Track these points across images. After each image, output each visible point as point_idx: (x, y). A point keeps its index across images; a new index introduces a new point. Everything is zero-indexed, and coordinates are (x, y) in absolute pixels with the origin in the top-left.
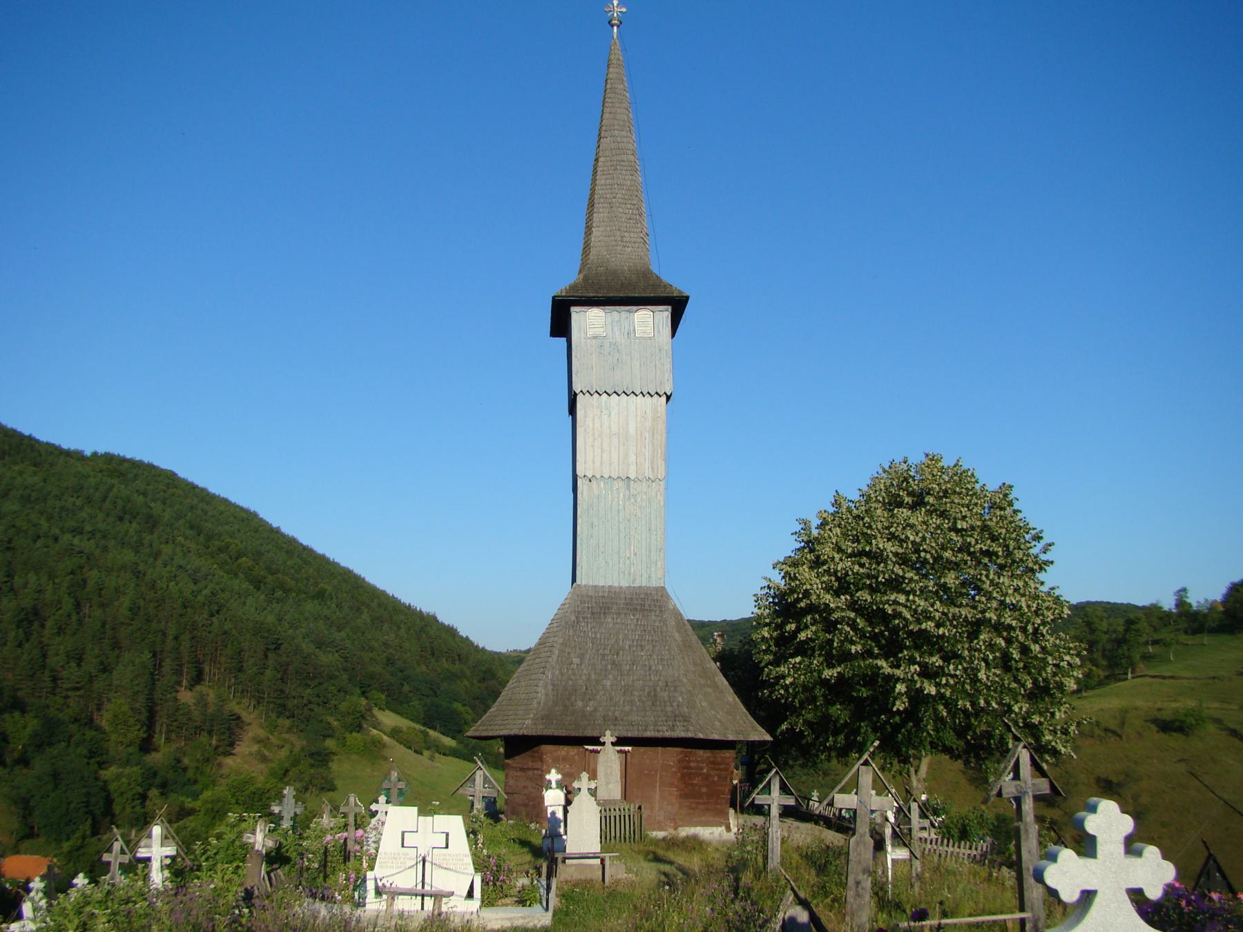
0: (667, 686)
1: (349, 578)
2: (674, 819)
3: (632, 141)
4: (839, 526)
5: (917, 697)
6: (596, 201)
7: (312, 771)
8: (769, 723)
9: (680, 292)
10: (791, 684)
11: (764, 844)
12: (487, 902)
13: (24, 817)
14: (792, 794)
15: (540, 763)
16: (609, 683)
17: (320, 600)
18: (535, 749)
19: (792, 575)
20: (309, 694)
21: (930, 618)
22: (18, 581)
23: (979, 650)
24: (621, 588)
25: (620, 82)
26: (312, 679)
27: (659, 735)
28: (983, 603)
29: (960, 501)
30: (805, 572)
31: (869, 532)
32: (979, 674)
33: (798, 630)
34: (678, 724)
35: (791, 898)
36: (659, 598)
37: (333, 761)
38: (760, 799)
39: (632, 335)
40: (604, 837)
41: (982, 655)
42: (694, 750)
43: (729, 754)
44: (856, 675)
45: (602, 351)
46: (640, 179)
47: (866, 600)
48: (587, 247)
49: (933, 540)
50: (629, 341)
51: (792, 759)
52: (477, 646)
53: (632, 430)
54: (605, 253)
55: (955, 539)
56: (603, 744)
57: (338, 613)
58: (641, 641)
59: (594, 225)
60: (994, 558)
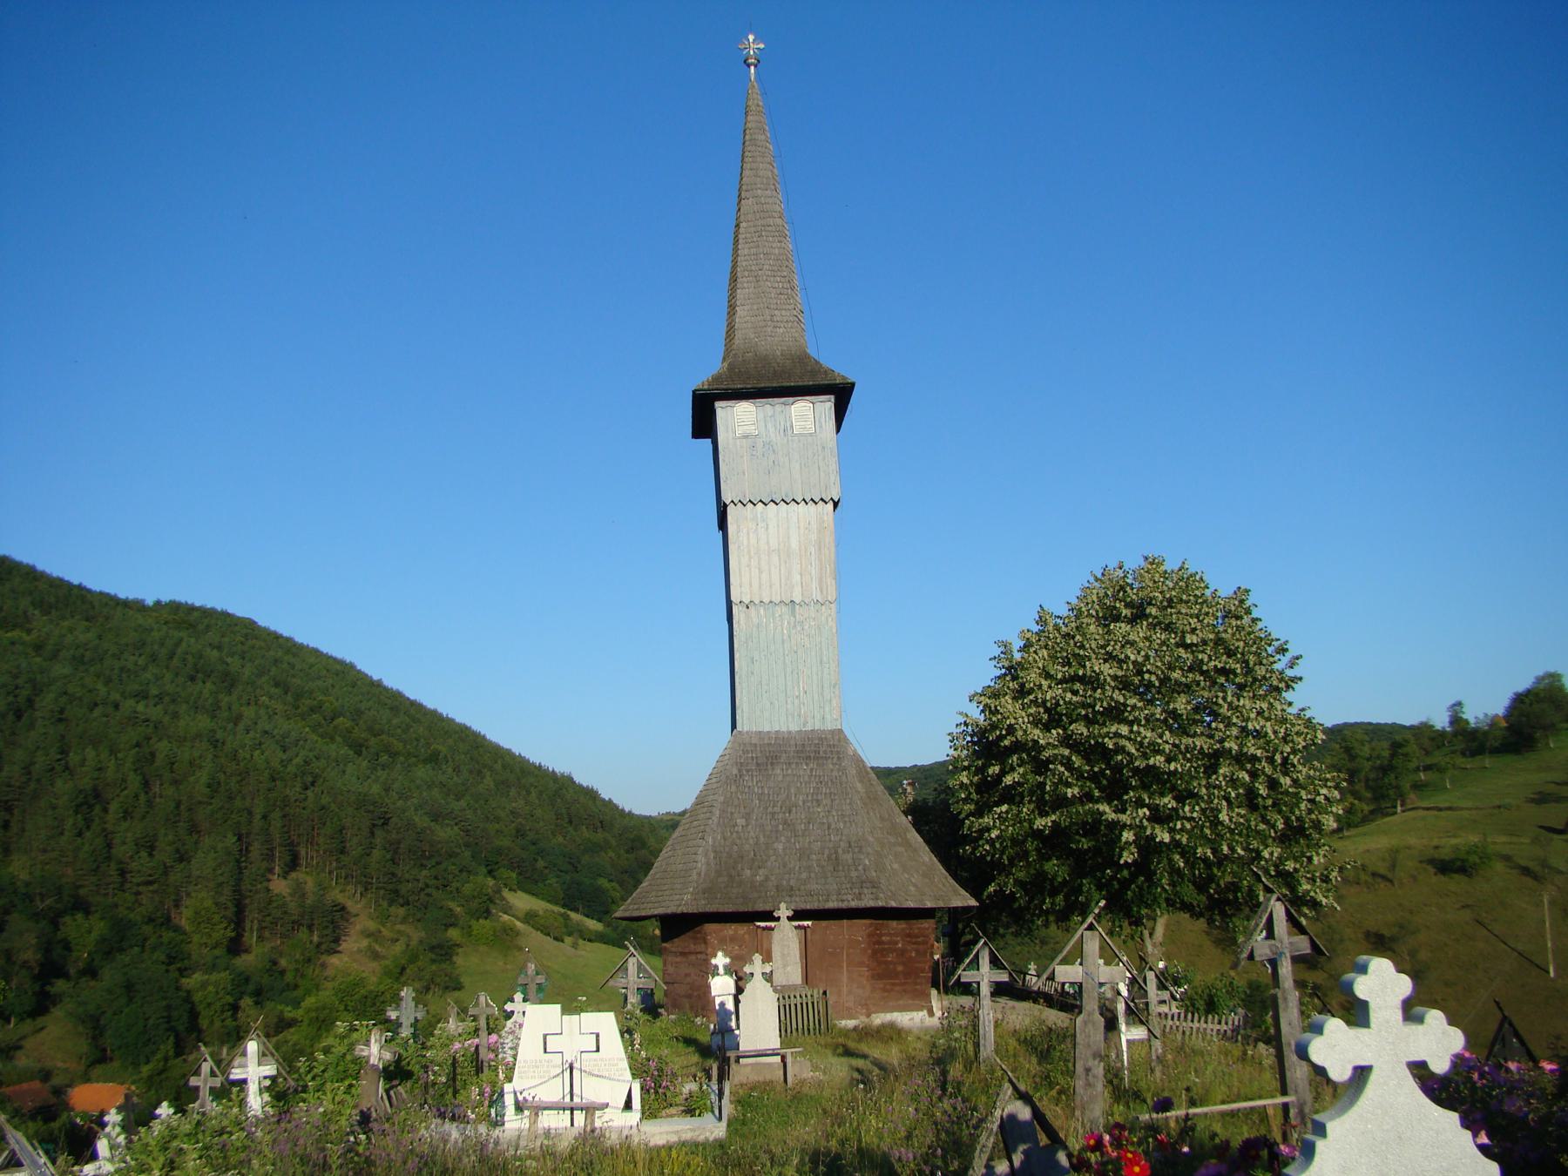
0: (850, 846)
1: (467, 736)
2: (866, 1004)
4: (1046, 647)
5: (1148, 847)
10: (998, 837)
12: (649, 1113)
14: (1005, 968)
15: (703, 945)
16: (780, 847)
20: (425, 876)
21: (1159, 752)
22: (74, 758)
23: (1219, 787)
24: (790, 732)
27: (844, 905)
28: (1221, 730)
29: (1188, 611)
30: (1008, 704)
31: (1082, 652)
32: (1220, 816)
33: (1003, 773)
34: (866, 891)
35: (1010, 1091)
37: (457, 954)
38: (967, 976)
39: (790, 432)
40: (784, 1030)
41: (1222, 793)
42: (885, 922)
43: (928, 924)
52: (623, 810)
53: (794, 544)
54: (752, 336)
56: (778, 919)
57: (455, 778)
58: (817, 794)
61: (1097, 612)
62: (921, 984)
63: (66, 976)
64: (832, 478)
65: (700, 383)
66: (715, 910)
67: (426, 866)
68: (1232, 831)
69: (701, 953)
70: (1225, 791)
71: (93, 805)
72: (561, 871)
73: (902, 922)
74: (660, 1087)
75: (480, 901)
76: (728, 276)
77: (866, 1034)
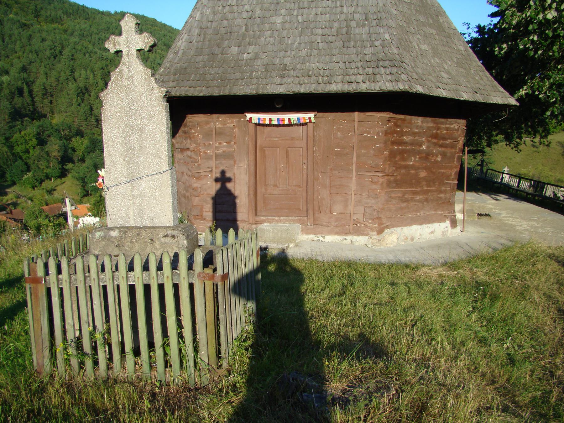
2: (379, 218)
13: (84, 186)
16: (279, 20)
22: (76, 74)
34: (382, 70)
42: (408, 117)
62: (445, 192)
63: (73, 162)
71: (85, 93)
73: (429, 119)
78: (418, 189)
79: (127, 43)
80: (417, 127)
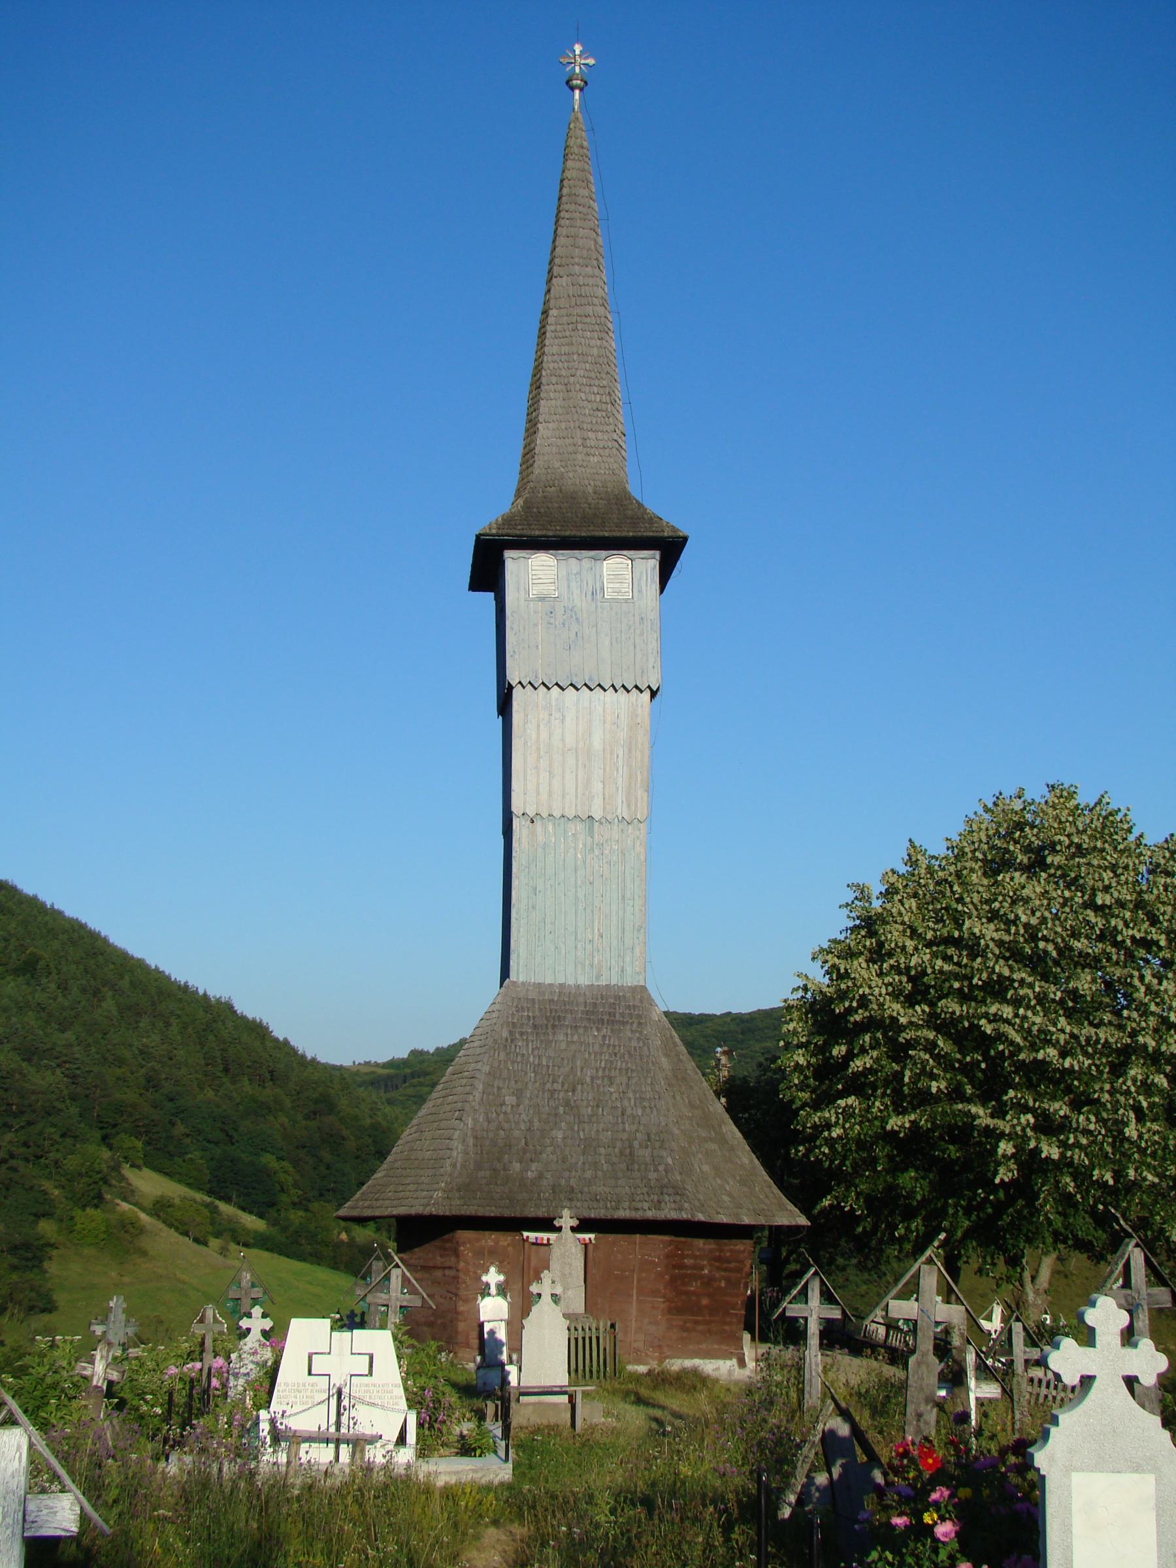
0: (649, 1140)
1: (81, 938)
2: (660, 1346)
3: (601, 284)
4: (915, 895)
5: (1030, 1162)
6: (544, 380)
7: (15, 1277)
8: (803, 1198)
9: (674, 529)
10: (840, 1137)
11: (799, 1373)
12: (423, 1451)
14: (837, 1303)
15: (453, 1259)
16: (560, 1135)
17: (28, 976)
18: (447, 1236)
19: (842, 971)
20: (10, 1142)
21: (1048, 1042)
23: (1127, 1093)
24: (578, 987)
25: (584, 184)
26: (15, 1115)
27: (638, 1215)
28: (1135, 1020)
29: (1101, 862)
30: (860, 968)
31: (960, 908)
32: (1126, 1130)
33: (850, 1056)
34: (667, 1198)
35: (833, 1406)
36: (637, 1003)
37: (50, 1258)
38: (794, 1310)
39: (599, 596)
40: (573, 1371)
41: (1131, 1102)
42: (689, 1240)
43: (742, 1246)
44: (939, 1126)
45: (552, 621)
46: (613, 344)
47: (953, 1013)
48: (528, 455)
49: (1057, 922)
50: (594, 605)
51: (843, 1255)
52: (303, 1056)
53: (597, 743)
54: (557, 464)
55: (1093, 920)
56: (559, 1229)
57: (60, 999)
58: (610, 1070)
59: (541, 419)
60: (1155, 949)
61: (984, 854)
64: (651, 660)
65: (486, 524)
66: (473, 1213)
67: (11, 1127)
68: (1142, 1151)
69: (450, 1268)
70: (1134, 1099)
72: (209, 1142)
73: (711, 1241)
74: (436, 1421)
75: (91, 1181)
76: (529, 380)
77: (663, 1380)
78: (700, 1318)
79: (565, 1223)
80: (699, 1250)
